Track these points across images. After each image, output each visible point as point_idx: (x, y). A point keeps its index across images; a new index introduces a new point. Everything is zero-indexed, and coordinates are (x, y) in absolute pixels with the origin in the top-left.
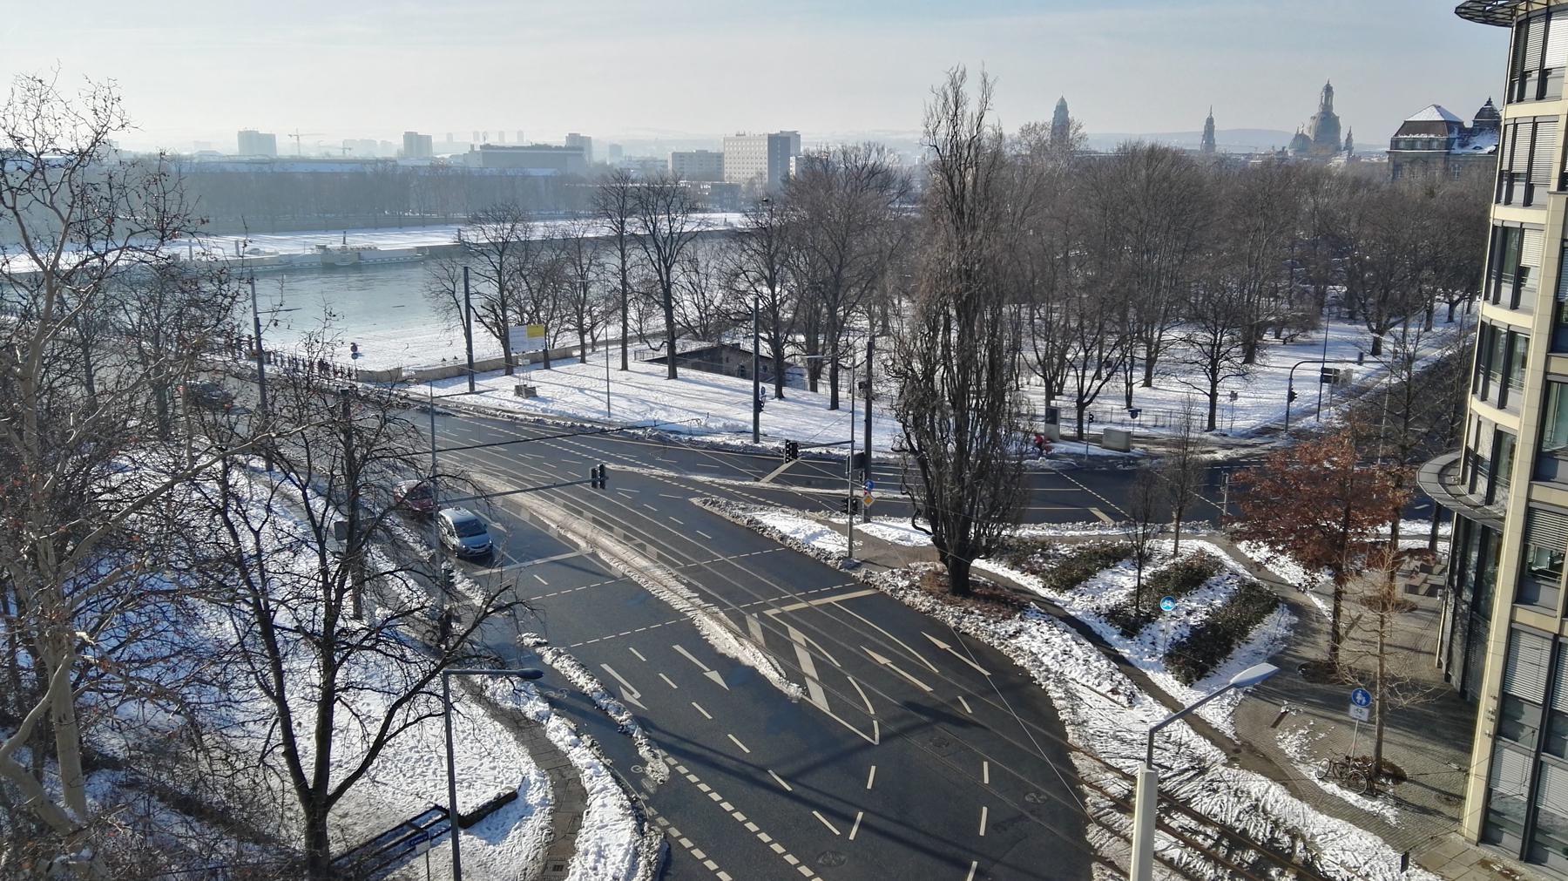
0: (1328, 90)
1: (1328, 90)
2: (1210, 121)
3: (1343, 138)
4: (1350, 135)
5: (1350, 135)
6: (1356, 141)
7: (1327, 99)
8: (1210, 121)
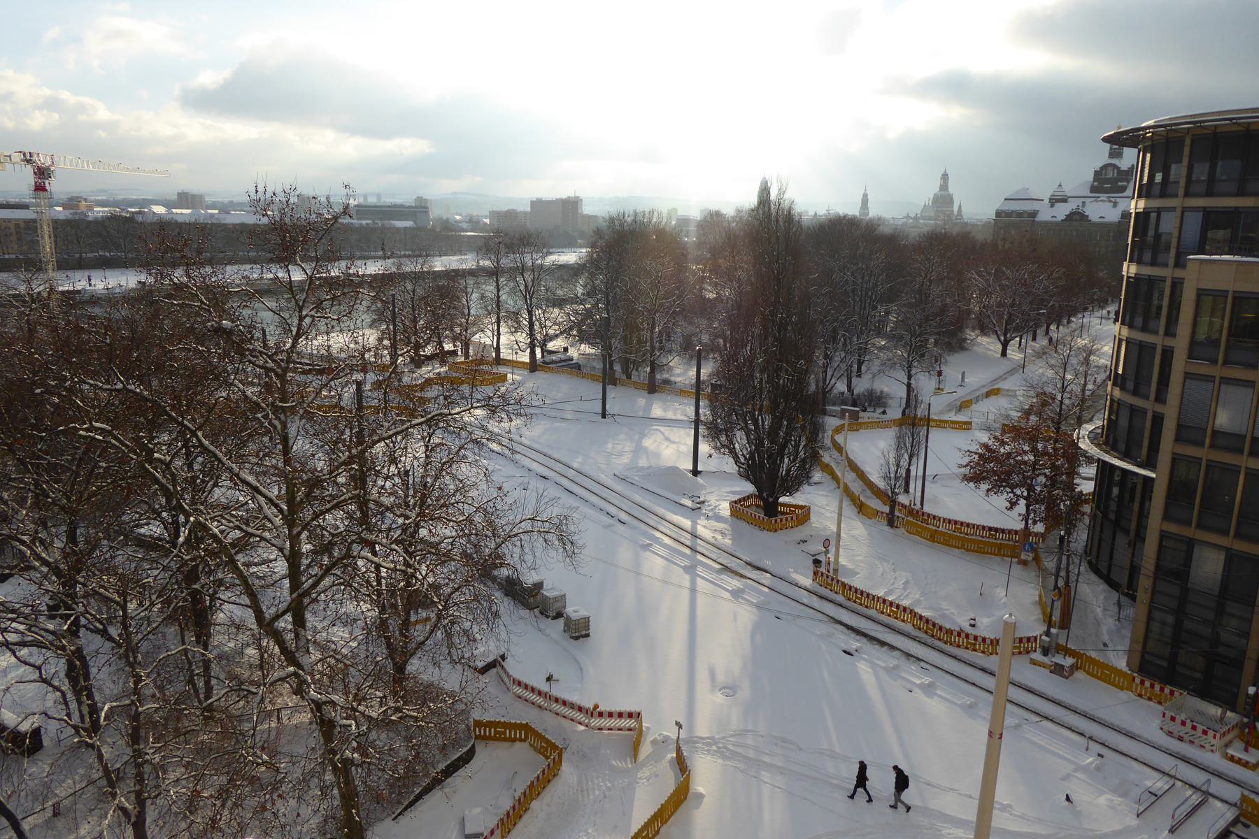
0: (945, 177)
1: (945, 177)
3: (956, 209)
4: (960, 207)
5: (960, 207)
6: (964, 210)
7: (944, 182)
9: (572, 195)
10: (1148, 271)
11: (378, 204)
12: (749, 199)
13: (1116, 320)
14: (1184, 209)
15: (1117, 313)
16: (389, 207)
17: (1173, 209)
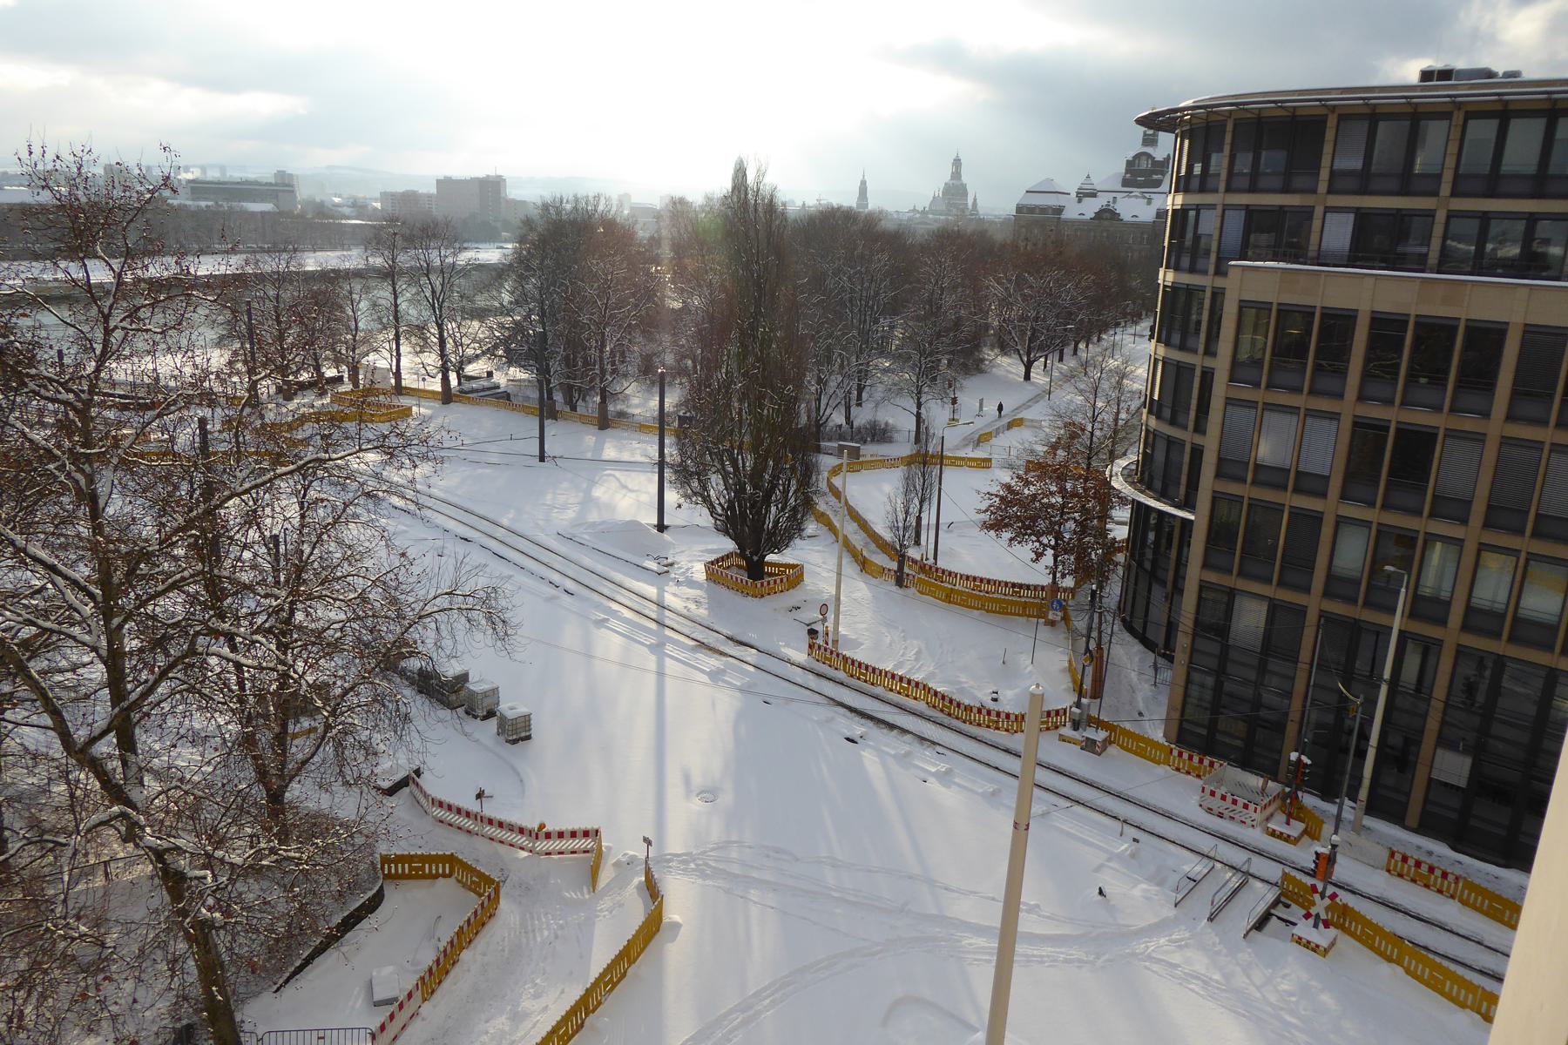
0: (957, 163)
1: (957, 163)
2: (863, 183)
3: (970, 201)
4: (975, 200)
5: (975, 200)
8: (863, 183)
9: (492, 173)
10: (1187, 279)
11: (222, 180)
12: (721, 185)
13: (1151, 337)
14: (1226, 207)
15: (1152, 329)
16: (238, 183)
17: (1212, 207)
